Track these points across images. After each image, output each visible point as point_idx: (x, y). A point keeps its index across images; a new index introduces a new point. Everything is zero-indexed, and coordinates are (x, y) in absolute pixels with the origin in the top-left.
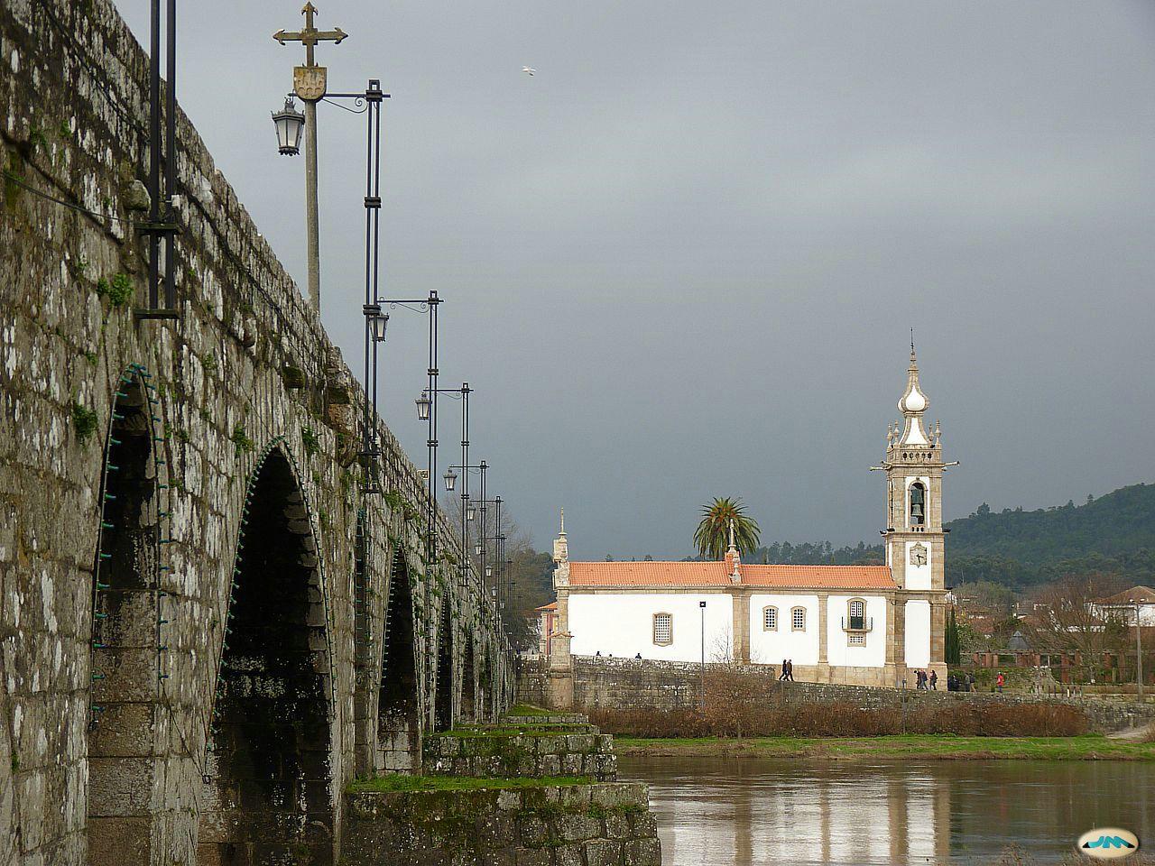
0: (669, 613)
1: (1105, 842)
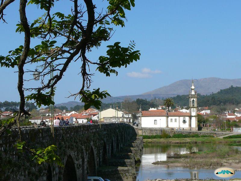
1: (223, 172)
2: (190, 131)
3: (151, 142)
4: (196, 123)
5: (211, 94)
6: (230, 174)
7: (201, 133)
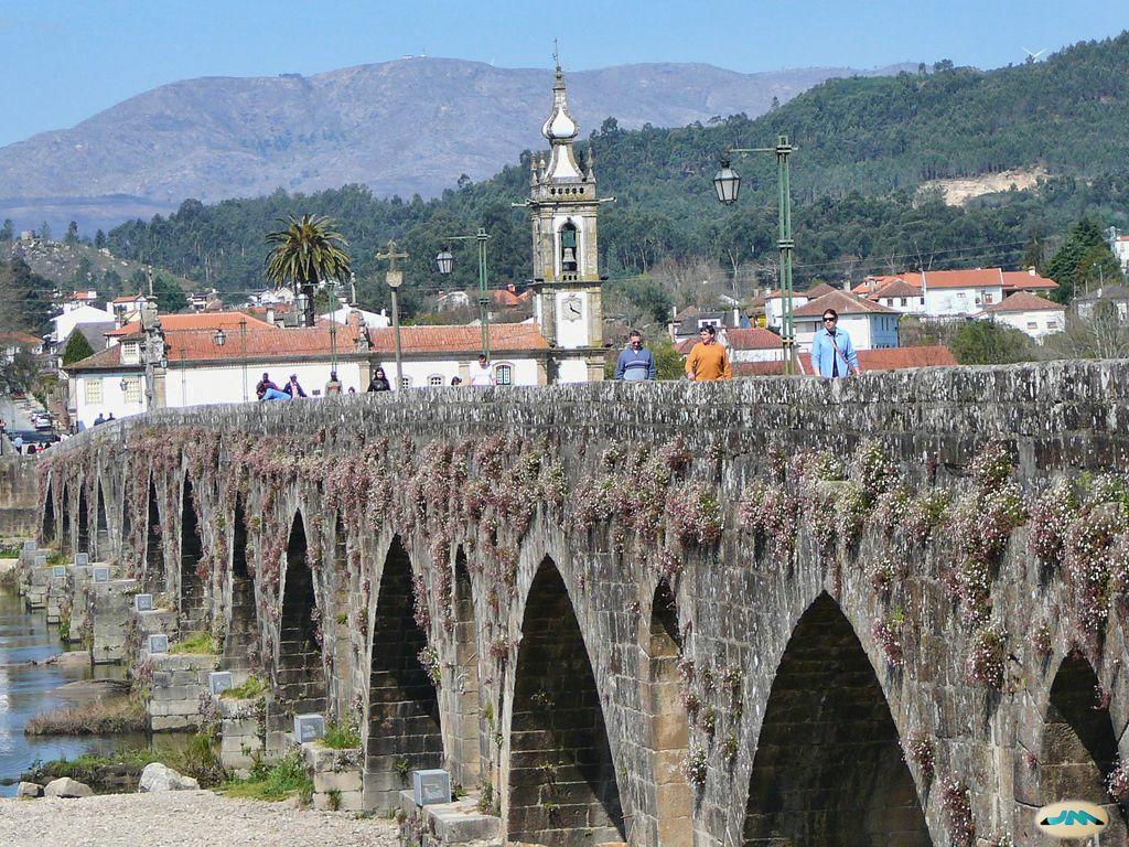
1: (1068, 818)
5: (449, 193)
6: (1091, 824)
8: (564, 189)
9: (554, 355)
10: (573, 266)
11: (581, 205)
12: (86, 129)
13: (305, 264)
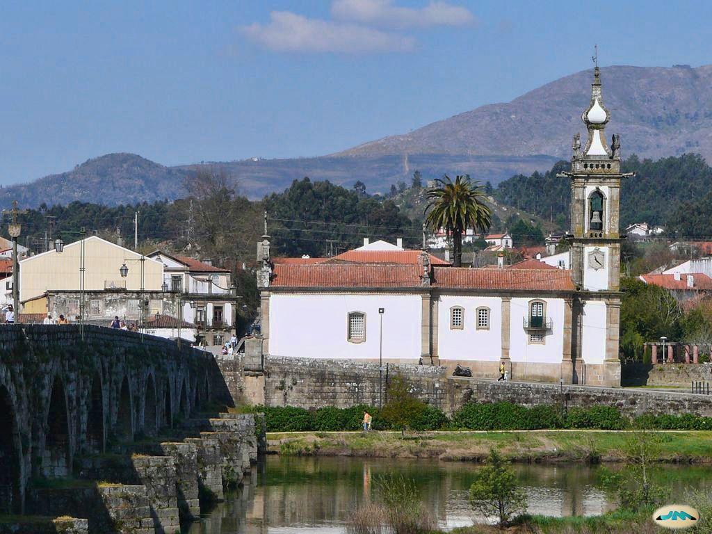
0: (362, 310)
1: (673, 516)
2: (570, 387)
3: (314, 454)
4: (609, 339)
7: (633, 403)
8: (595, 164)
9: (580, 296)
10: (599, 226)
11: (608, 178)
12: (522, 104)
13: (454, 215)
